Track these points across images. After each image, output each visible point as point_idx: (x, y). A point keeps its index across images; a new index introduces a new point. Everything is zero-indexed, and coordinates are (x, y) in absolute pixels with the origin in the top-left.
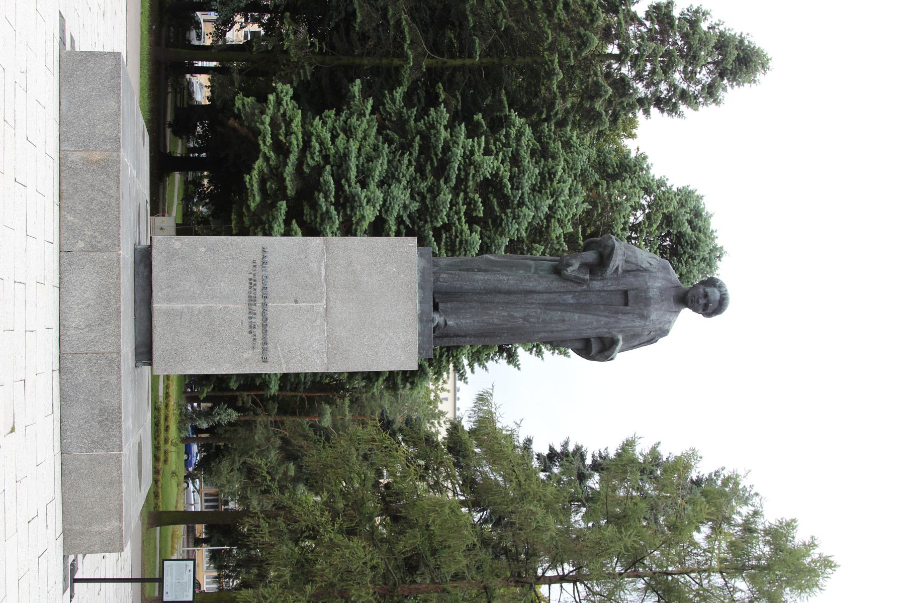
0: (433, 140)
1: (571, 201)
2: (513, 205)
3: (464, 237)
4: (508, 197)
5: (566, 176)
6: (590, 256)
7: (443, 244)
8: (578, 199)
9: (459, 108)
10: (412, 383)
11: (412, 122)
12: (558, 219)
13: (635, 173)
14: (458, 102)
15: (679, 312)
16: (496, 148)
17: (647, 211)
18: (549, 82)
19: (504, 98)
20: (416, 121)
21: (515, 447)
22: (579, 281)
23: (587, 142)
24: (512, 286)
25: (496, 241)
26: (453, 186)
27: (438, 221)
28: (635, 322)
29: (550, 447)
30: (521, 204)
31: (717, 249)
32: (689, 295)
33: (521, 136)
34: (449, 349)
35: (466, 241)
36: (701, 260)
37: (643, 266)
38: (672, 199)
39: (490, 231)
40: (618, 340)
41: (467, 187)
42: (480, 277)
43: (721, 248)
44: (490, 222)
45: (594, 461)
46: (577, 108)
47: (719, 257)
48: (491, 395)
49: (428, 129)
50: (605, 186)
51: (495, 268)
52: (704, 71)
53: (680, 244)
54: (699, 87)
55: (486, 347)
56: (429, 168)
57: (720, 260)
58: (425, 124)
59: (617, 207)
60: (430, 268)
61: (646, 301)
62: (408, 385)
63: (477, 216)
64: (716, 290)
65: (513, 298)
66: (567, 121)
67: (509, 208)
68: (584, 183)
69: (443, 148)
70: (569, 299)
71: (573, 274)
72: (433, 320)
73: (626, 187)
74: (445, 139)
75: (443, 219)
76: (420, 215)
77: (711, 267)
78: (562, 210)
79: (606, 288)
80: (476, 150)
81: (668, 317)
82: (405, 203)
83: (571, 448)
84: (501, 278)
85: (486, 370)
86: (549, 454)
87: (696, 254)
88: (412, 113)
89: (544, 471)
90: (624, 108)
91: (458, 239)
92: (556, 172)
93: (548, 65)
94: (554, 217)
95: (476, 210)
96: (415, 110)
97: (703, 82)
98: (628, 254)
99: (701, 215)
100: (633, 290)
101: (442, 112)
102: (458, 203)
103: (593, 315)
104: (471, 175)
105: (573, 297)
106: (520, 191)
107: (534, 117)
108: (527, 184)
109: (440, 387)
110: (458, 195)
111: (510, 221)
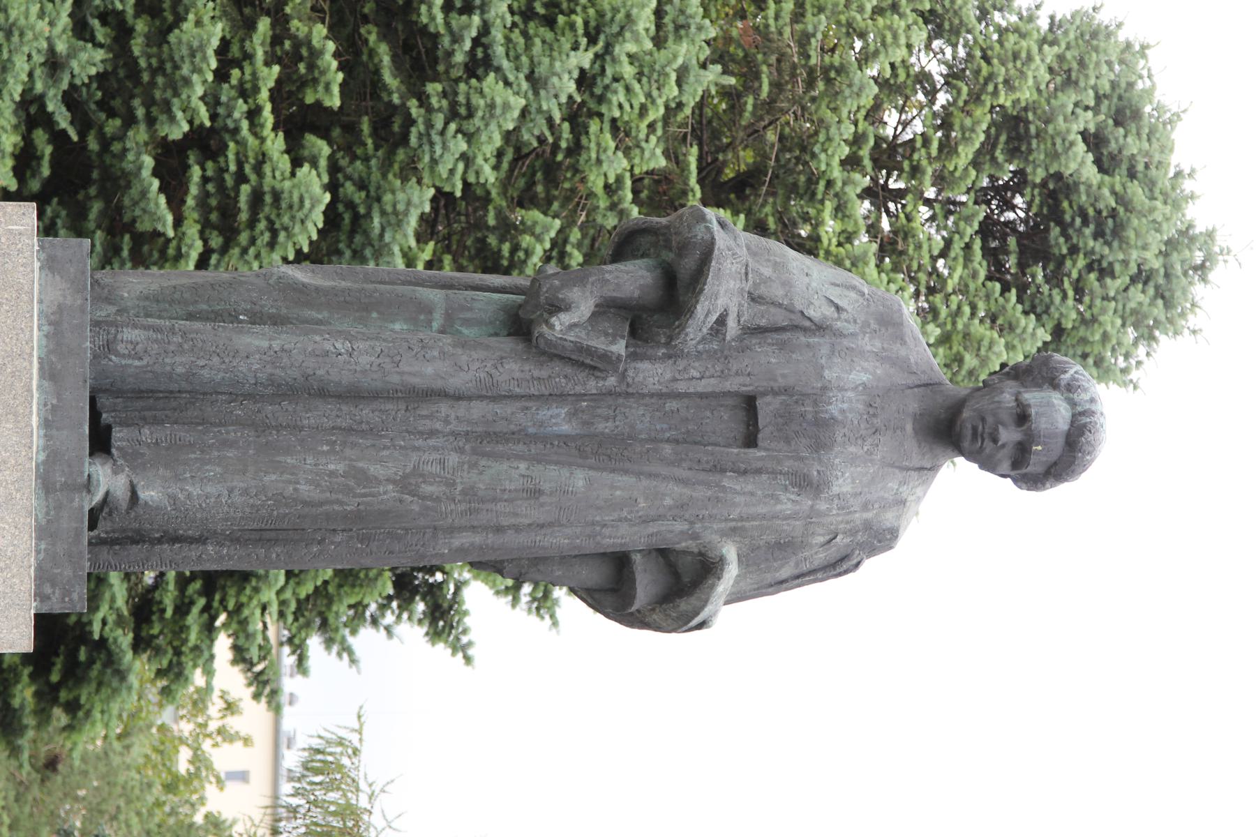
1: (662, 56)
2: (450, 66)
3: (268, 182)
4: (436, 36)
7: (190, 202)
8: (685, 51)
10: (72, 707)
15: (934, 469)
17: (942, 98)
24: (364, 372)
25: (388, 198)
27: (172, 119)
28: (778, 501)
30: (479, 65)
31: (1193, 239)
32: (966, 414)
34: (212, 582)
35: (277, 196)
36: (1134, 280)
37: (811, 313)
38: (1030, 58)
39: (366, 159)
42: (256, 340)
43: (1210, 235)
44: (366, 127)
47: (1202, 267)
48: (356, 752)
51: (315, 315)
55: (347, 578)
57: (1204, 279)
59: (829, 81)
62: (58, 712)
63: (318, 104)
64: (1057, 399)
65: (366, 413)
67: (436, 78)
70: (559, 420)
71: (571, 337)
72: (88, 485)
73: (861, 9)
76: (108, 95)
77: (1168, 305)
78: (628, 89)
79: (681, 387)
81: (893, 485)
82: (51, 50)
84: (328, 346)
85: (353, 661)
91: (245, 189)
94: (600, 115)
95: (315, 81)
98: (756, 272)
99: (1137, 115)
100: (775, 393)
102: (249, 57)
103: (638, 474)
106: (476, 19)
109: (213, 726)
110: (251, 26)
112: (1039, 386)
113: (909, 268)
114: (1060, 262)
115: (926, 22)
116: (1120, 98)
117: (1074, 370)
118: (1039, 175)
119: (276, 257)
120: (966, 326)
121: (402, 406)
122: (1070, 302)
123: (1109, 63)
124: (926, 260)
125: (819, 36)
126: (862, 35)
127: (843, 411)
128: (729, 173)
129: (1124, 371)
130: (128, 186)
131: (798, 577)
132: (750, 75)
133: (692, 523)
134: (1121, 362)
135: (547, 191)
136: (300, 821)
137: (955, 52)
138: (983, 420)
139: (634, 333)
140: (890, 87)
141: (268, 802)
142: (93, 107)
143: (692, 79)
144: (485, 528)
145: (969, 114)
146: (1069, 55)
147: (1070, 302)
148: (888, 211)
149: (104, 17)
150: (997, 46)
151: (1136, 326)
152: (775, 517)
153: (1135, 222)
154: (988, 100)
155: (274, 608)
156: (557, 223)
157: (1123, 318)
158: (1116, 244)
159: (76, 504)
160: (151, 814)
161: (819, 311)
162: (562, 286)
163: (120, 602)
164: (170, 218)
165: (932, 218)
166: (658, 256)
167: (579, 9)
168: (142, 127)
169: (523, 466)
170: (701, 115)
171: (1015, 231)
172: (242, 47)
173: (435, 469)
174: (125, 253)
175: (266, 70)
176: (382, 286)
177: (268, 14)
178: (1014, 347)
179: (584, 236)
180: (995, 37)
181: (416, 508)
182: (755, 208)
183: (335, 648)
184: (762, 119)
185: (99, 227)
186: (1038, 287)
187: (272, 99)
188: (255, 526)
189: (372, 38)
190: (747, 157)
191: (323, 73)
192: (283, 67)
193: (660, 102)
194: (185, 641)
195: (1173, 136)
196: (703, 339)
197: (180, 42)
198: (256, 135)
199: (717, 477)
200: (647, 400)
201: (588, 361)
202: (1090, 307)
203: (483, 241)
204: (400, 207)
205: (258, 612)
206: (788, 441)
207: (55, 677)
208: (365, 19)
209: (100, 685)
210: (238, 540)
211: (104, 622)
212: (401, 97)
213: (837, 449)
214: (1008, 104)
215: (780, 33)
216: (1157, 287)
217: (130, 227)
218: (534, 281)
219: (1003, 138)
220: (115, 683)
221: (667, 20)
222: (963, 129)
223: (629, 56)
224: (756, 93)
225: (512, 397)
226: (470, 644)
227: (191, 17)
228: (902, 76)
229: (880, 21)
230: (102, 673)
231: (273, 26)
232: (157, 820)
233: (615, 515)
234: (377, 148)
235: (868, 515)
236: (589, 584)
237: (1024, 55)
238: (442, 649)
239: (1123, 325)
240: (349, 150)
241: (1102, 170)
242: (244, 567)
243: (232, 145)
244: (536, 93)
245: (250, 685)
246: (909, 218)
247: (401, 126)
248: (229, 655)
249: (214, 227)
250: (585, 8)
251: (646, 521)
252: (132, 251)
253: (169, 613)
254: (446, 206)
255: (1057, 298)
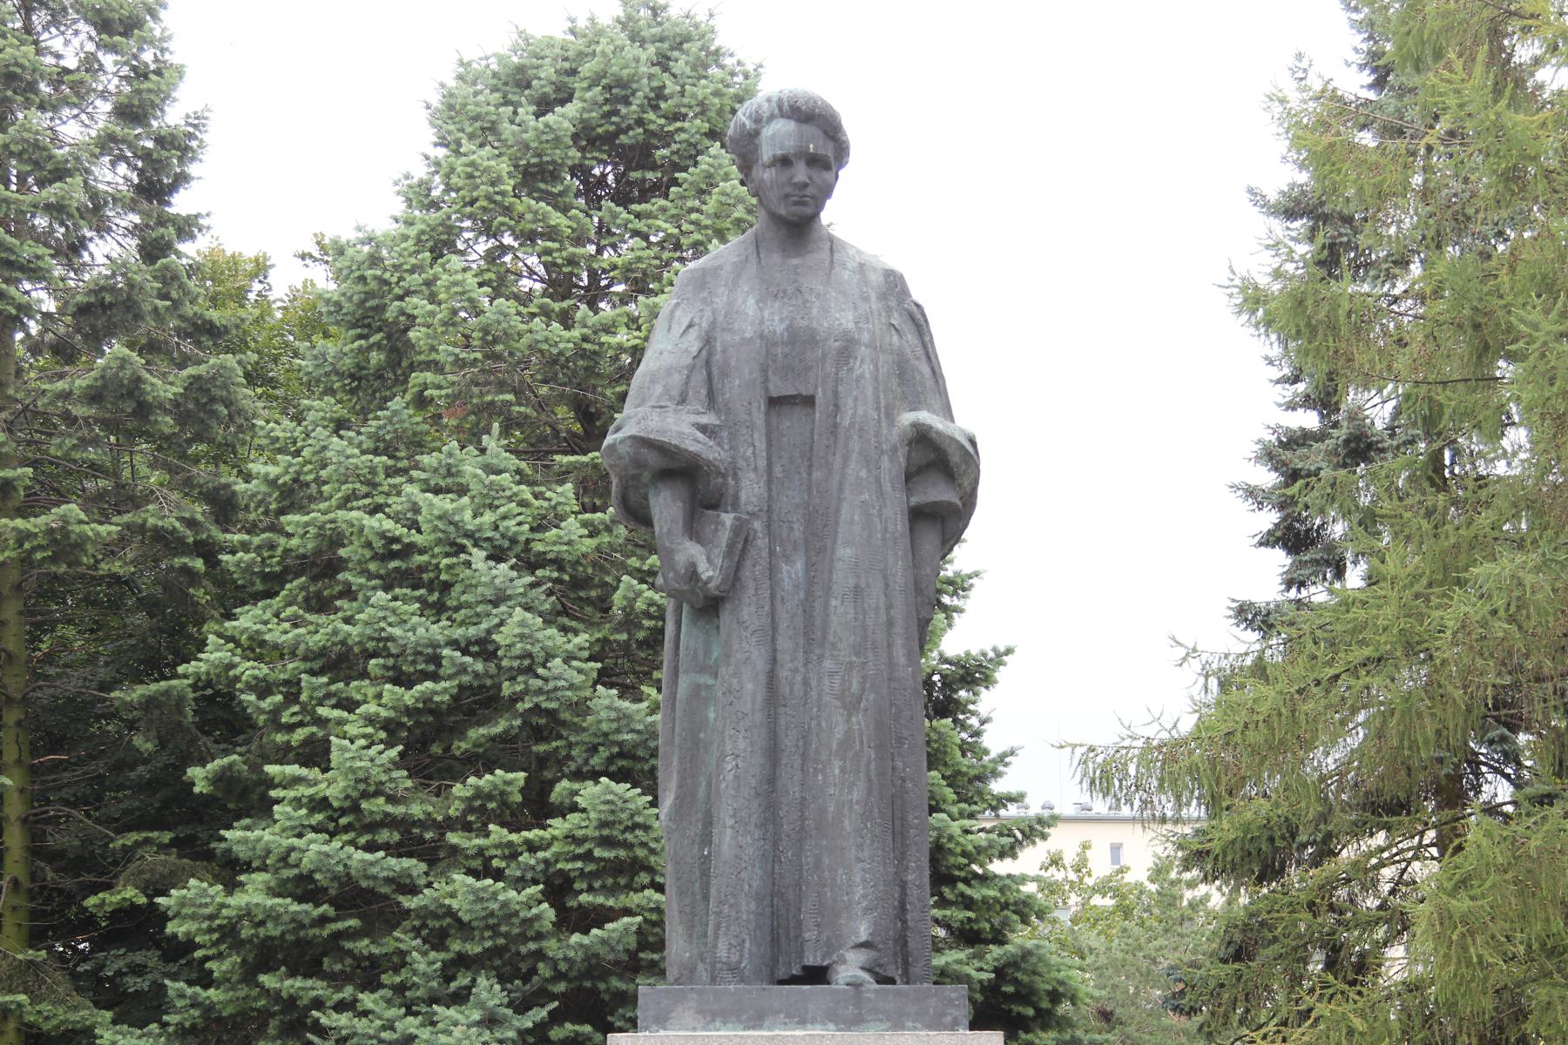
0: (272, 930)
1: (475, 487)
2: (487, 674)
3: (589, 832)
4: (460, 686)
5: (397, 504)
6: (666, 507)
7: (611, 902)
8: (470, 467)
9: (167, 837)
10: (1055, 997)
11: (211, 992)
12: (532, 529)
13: (387, 283)
14: (147, 841)
15: (831, 239)
16: (301, 724)
17: (508, 240)
18: (90, 548)
19: (140, 692)
20: (207, 981)
21: (1260, 669)
22: (741, 544)
23: (284, 428)
24: (752, 744)
25: (605, 727)
26: (423, 867)
27: (538, 917)
28: (862, 376)
29: (1261, 544)
30: (485, 648)
31: (629, 18)
32: (782, 211)
33: (262, 643)
34: (942, 877)
35: (603, 824)
36: (666, 69)
37: (695, 349)
38: (472, 164)
39: (570, 746)
40: (916, 425)
41: (428, 822)
42: (726, 840)
44: (541, 748)
45: (1307, 402)
46: (170, 452)
48: (1091, 749)
49: (238, 945)
50: (429, 376)
52: (57, 44)
53: (616, 134)
54: (108, 60)
55: (935, 759)
56: (363, 946)
57: (665, 8)
58: (220, 956)
59: (495, 341)
60: (700, 993)
61: (801, 341)
63: (522, 791)
64: (768, 132)
65: (789, 741)
66: (217, 489)
68: (418, 444)
69: (300, 899)
70: (793, 571)
71: (718, 561)
72: (856, 985)
73: (432, 314)
74: (273, 892)
75: (530, 897)
76: (517, 973)
77: (688, 38)
78: (504, 517)
79: (762, 463)
80: (311, 791)
81: (846, 275)
83: (1267, 478)
84: (730, 777)
86: (1285, 546)
87: (644, 89)
88: (182, 996)
89: (1340, 573)
90: (176, 304)
91: (598, 853)
92: (382, 535)
93: (34, 549)
94: (528, 541)
95: (503, 793)
96: (173, 986)
97: (91, 47)
98: (659, 398)
99: (521, 69)
100: (766, 380)
101: (182, 903)
102: (481, 851)
103: (840, 500)
104: (390, 809)
105: (788, 559)
106: (446, 652)
107: (200, 595)
108: (421, 631)
109: (1072, 876)
110: (454, 849)
111: (539, 683)
112: (757, 148)
113: (657, 267)
114: (652, 134)
115: (442, 256)
116: (506, 84)
117: (743, 115)
118: (574, 153)
119: (656, 824)
120: (708, 216)
121: (782, 710)
122: (686, 125)
123: (476, 94)
124: (651, 253)
125: (457, 351)
126: (455, 312)
127: (781, 320)
128: (577, 428)
129: (746, 77)
130: (596, 955)
131: (929, 358)
132: (491, 409)
133: (882, 452)
134: (739, 79)
135: (596, 587)
136: (1156, 800)
137: (467, 229)
138: (787, 196)
139: (715, 505)
140: (499, 285)
141: (1138, 827)
142: (527, 987)
143: (495, 461)
144: (889, 634)
145: (521, 216)
146: (469, 130)
147: (686, 125)
148: (608, 286)
149: (448, 979)
150: (462, 193)
151: (706, 67)
152: (876, 378)
153: (615, 69)
154: (510, 200)
155: (967, 823)
156: (625, 578)
157: (699, 79)
158: (634, 86)
159: (872, 996)
160: (1151, 929)
161: (693, 343)
162: (674, 569)
163: (961, 955)
164: (626, 920)
165: (614, 246)
166: (646, 485)
167: (434, 561)
168: (545, 944)
169: (834, 603)
170: (525, 452)
171: (624, 174)
172: (473, 857)
173: (837, 680)
174: (656, 956)
175: (492, 836)
176: (677, 729)
177: (443, 835)
178: (726, 174)
179: (633, 554)
180: (453, 195)
181: (872, 697)
182: (607, 402)
183: (1001, 768)
184: (528, 399)
185: (633, 981)
186: (673, 153)
187: (518, 830)
188: (890, 838)
189: (464, 745)
190: (562, 412)
191: (495, 786)
192: (489, 821)
193: (516, 489)
194: (996, 900)
195: (539, 36)
196: (719, 444)
197: (470, 911)
198: (549, 845)
199: (842, 435)
200: (774, 494)
201: (740, 546)
202: (691, 107)
203: (641, 644)
204: (613, 715)
205: (970, 837)
206: (808, 369)
207: (1030, 1012)
208: (447, 749)
209: (1035, 973)
210: (903, 853)
211: (980, 969)
212: (515, 718)
213: (815, 325)
214: (512, 182)
215: (453, 383)
216: (672, 49)
217: (633, 955)
218: (670, 595)
219: (542, 186)
220: (1034, 960)
221: (443, 484)
222: (535, 221)
223: (475, 516)
224: (509, 404)
225: (773, 613)
226: (995, 650)
227: (447, 901)
228: (491, 276)
229: (442, 296)
230: (1025, 972)
231: (453, 830)
232: (1156, 924)
233: (876, 520)
234: (560, 737)
235: (873, 297)
236: (937, 542)
237: (469, 170)
238: (1001, 674)
239: (706, 77)
240: (560, 763)
241: (569, 99)
242: (926, 848)
243: (559, 866)
244: (509, 598)
245: (1034, 843)
246: (614, 267)
247: (540, 716)
248: (1008, 861)
249: (632, 879)
250: (433, 556)
251: (881, 493)
252: (654, 951)
253: (971, 914)
254: (609, 676)
255: (683, 136)
